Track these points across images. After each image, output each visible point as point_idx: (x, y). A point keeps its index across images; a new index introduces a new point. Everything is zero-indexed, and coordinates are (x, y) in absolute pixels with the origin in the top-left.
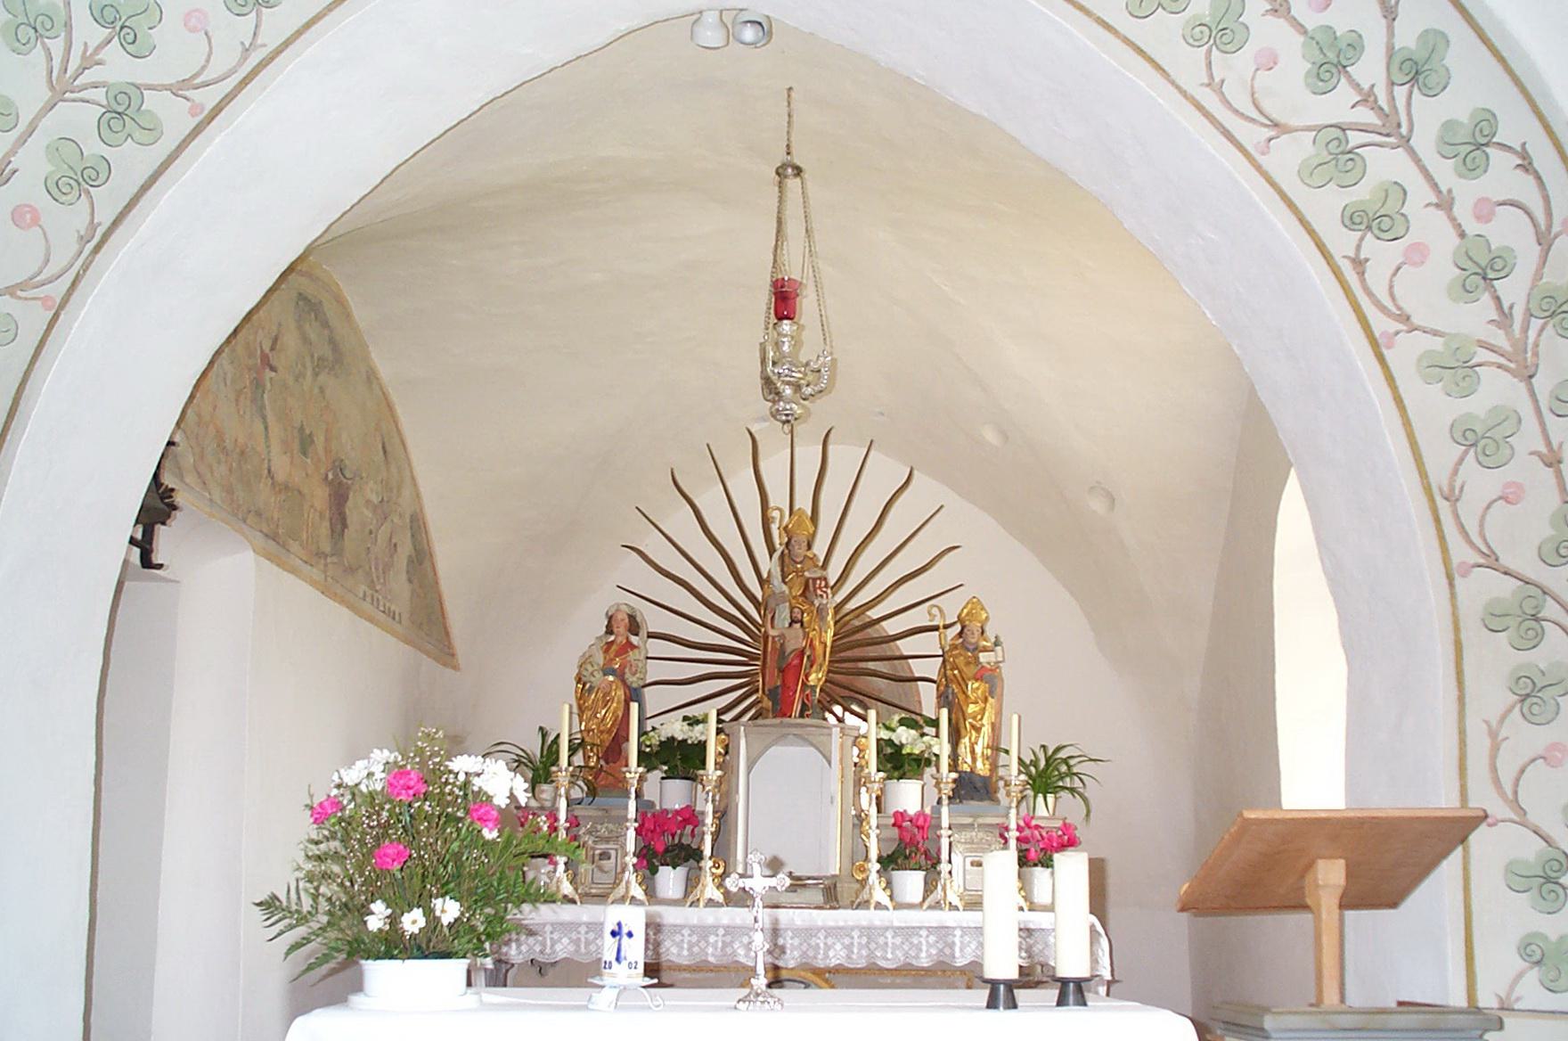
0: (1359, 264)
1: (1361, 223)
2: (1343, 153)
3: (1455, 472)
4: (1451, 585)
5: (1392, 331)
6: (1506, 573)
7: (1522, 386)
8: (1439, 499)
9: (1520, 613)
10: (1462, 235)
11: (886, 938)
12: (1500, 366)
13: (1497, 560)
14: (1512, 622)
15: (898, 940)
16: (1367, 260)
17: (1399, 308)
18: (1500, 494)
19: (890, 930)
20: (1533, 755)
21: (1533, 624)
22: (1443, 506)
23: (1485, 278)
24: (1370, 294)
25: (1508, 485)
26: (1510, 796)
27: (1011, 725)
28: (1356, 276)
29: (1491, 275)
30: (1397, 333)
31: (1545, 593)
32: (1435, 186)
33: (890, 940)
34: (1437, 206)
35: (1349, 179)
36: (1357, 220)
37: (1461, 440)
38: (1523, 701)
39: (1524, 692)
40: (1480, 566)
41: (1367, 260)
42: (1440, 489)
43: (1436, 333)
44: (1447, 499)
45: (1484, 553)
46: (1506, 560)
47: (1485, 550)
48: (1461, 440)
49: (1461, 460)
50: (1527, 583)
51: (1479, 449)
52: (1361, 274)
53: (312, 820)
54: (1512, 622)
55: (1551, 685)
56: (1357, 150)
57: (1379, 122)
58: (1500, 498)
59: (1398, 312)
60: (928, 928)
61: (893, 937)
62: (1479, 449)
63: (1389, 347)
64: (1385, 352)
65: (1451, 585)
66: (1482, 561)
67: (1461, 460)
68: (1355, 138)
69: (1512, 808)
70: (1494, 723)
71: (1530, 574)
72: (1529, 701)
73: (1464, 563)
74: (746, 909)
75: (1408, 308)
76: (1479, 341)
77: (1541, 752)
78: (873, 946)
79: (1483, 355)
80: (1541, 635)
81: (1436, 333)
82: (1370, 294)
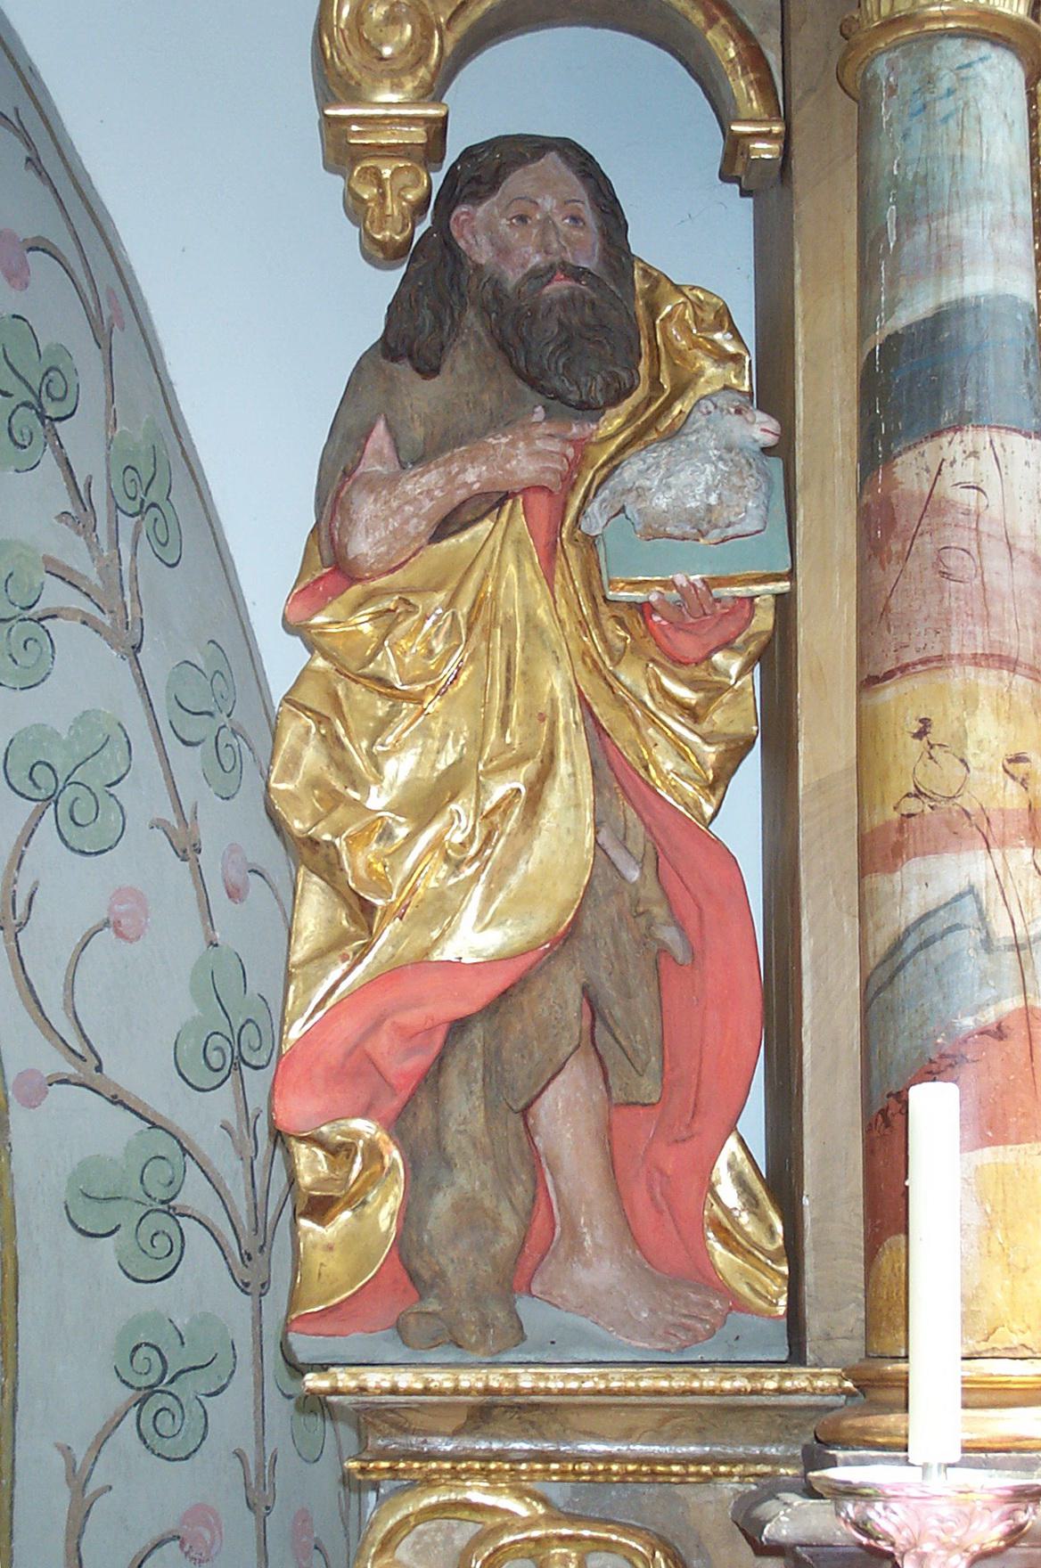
6: (115, 1101)
7: (125, 667)
9: (141, 1196)
13: (99, 1069)
14: (126, 1215)
19: (292, 1337)
20: (156, 1534)
21: (164, 1222)
23: (42, 416)
25: (121, 894)
29: (52, 410)
31: (185, 1151)
37: (27, 787)
38: (142, 1402)
39: (144, 1381)
40: (66, 1082)
46: (117, 1072)
48: (27, 787)
50: (154, 1125)
53: (992, 807)
54: (126, 1215)
55: (194, 1368)
58: (106, 923)
66: (69, 1070)
70: (80, 1455)
71: (160, 1107)
72: (157, 1402)
73: (32, 1071)
76: (48, 560)
77: (170, 1524)
79: (56, 594)
80: (178, 1249)
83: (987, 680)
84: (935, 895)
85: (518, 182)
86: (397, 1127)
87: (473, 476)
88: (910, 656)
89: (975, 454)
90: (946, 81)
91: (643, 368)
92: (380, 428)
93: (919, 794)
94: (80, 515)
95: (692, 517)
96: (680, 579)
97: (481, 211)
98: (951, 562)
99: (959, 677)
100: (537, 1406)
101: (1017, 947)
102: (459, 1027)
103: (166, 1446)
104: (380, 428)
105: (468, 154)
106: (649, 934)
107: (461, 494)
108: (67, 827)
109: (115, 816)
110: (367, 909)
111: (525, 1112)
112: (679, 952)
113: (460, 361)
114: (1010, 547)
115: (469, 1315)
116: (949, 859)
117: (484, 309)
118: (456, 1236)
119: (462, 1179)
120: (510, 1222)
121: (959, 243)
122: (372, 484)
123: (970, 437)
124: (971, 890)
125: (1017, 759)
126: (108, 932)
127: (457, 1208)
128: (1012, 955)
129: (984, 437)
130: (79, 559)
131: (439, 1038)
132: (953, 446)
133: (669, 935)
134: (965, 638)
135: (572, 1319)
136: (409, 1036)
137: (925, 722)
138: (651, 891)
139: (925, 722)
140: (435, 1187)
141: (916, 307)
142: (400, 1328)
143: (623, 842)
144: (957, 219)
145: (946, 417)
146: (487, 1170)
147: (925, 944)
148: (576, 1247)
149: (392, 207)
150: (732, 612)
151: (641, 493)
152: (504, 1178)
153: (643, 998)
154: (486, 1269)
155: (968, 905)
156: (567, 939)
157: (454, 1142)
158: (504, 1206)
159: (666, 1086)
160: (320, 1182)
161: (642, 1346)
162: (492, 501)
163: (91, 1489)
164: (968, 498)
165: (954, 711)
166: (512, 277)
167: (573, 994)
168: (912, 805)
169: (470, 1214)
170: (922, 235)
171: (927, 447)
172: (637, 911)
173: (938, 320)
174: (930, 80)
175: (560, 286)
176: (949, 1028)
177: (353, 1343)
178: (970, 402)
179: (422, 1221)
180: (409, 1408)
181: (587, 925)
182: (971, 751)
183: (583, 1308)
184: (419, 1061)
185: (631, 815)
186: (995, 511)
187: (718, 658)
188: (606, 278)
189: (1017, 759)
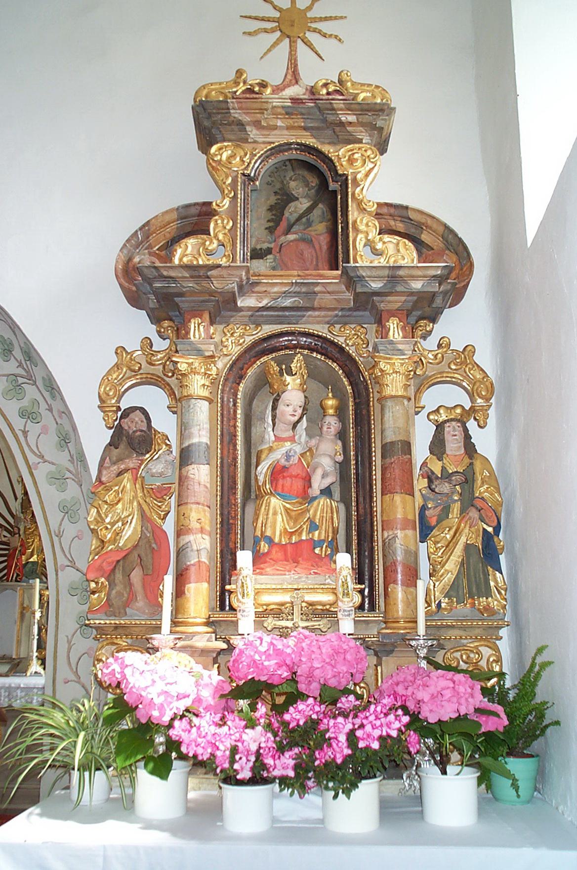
0: (25, 433)
1: (25, 416)
2: (17, 386)
3: (61, 525)
4: (57, 575)
5: (37, 462)
6: (77, 570)
8: (53, 536)
10: (57, 423)
11: (17, 693)
12: (73, 480)
14: (79, 592)
15: (23, 694)
16: (28, 431)
17: (40, 453)
18: (76, 535)
20: (83, 652)
22: (56, 539)
23: (65, 442)
24: (29, 446)
25: (79, 531)
26: (75, 670)
27: (34, 600)
28: (23, 438)
30: (39, 463)
32: (48, 404)
33: (19, 694)
34: (49, 410)
35: (20, 397)
36: (24, 414)
38: (81, 627)
41: (28, 431)
42: (55, 532)
43: (53, 464)
44: (57, 536)
45: (70, 560)
47: (71, 559)
49: (63, 520)
51: (69, 514)
52: (26, 437)
54: (79, 592)
56: (22, 385)
57: (26, 374)
58: (76, 536)
59: (39, 454)
60: (38, 688)
61: (21, 692)
62: (69, 514)
63: (35, 469)
64: (33, 471)
65: (57, 575)
66: (69, 564)
67: (63, 520)
68: (21, 380)
69: (75, 676)
74: (239, 621)
75: (43, 453)
76: (67, 468)
78: (11, 696)
79: (68, 475)
81: (53, 464)
82: (29, 446)
83: (194, 506)
84: (184, 542)
85: (132, 416)
86: (107, 579)
87: (122, 467)
88: (182, 503)
89: (193, 469)
90: (192, 406)
91: (153, 447)
92: (108, 458)
93: (183, 525)
94: (72, 461)
95: (160, 473)
96: (157, 484)
97: (126, 420)
98: (189, 487)
99: (189, 506)
100: (125, 627)
101: (198, 551)
102: (118, 561)
103: (85, 636)
104: (108, 458)
105: (125, 410)
106: (150, 546)
107: (120, 470)
108: (70, 519)
109: (78, 516)
110: (103, 541)
111: (129, 576)
112: (156, 548)
113: (122, 446)
114: (199, 484)
115: (117, 611)
116: (187, 536)
117: (126, 437)
118: (116, 598)
119: (117, 588)
120: (126, 595)
121: (193, 434)
122: (106, 468)
123: (193, 466)
124: (190, 542)
125: (199, 519)
126: (77, 538)
127: (116, 593)
128: (196, 552)
129: (195, 466)
130: (72, 469)
131: (114, 563)
132: (190, 467)
133: (154, 546)
134: (191, 499)
135: (136, 612)
136: (109, 563)
137: (184, 514)
138: (151, 537)
139: (184, 514)
140: (113, 589)
141: (186, 444)
142: (106, 613)
143: (147, 530)
144: (192, 430)
145: (189, 463)
146: (122, 586)
147: (182, 551)
148: (136, 600)
149: (110, 421)
150: (166, 489)
151: (151, 469)
152: (125, 587)
153: (150, 556)
154: (121, 603)
155: (189, 544)
156: (135, 547)
157: (117, 581)
158: (125, 592)
159: (153, 571)
160: (94, 588)
161: (146, 617)
162: (126, 470)
163: (72, 643)
164: (192, 476)
165: (189, 512)
166: (131, 432)
167: (136, 555)
168: (182, 527)
169: (119, 594)
170: (187, 432)
171: (186, 468)
172: (149, 542)
173: (189, 446)
174: (189, 406)
175: (138, 433)
176: (186, 564)
177: (98, 616)
178: (193, 460)
179: (110, 595)
180: (104, 627)
181: (140, 544)
182: (191, 518)
183: (137, 610)
184: (112, 567)
185: (149, 525)
186: (197, 478)
187: (165, 497)
188: (147, 431)
189: (199, 519)
